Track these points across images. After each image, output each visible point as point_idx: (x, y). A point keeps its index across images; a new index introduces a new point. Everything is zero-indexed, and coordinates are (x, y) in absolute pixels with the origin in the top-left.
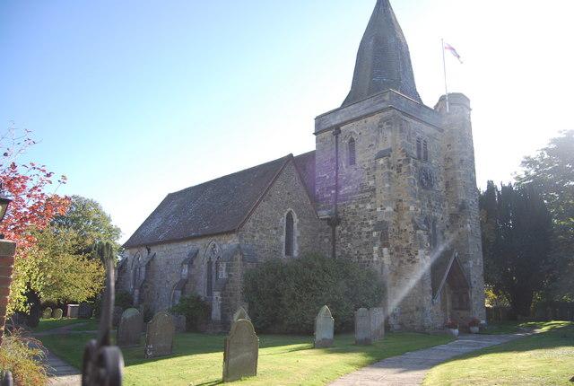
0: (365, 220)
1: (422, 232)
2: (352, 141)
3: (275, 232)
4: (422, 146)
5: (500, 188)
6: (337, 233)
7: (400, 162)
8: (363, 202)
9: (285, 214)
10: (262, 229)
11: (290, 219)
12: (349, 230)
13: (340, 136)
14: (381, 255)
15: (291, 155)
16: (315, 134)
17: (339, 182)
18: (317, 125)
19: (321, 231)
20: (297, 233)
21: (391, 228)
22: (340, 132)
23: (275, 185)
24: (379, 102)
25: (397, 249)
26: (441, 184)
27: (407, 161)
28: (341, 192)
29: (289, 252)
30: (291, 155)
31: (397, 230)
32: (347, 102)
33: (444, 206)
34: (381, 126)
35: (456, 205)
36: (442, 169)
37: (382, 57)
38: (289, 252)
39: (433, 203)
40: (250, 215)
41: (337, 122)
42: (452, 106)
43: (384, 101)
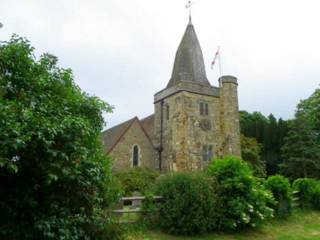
1: (192, 154)
3: (126, 156)
4: (204, 108)
5: (277, 121)
9: (133, 147)
10: (119, 156)
11: (136, 149)
14: (172, 167)
15: (136, 118)
16: (155, 103)
18: (155, 99)
19: (154, 155)
20: (140, 156)
21: (178, 153)
25: (182, 163)
26: (217, 127)
27: (187, 118)
28: (164, 134)
29: (135, 163)
30: (136, 118)
31: (182, 153)
32: (169, 86)
33: (218, 138)
34: (176, 101)
36: (218, 119)
37: (187, 56)
38: (135, 163)
39: (210, 138)
41: (162, 97)
42: (224, 84)
43: (179, 87)
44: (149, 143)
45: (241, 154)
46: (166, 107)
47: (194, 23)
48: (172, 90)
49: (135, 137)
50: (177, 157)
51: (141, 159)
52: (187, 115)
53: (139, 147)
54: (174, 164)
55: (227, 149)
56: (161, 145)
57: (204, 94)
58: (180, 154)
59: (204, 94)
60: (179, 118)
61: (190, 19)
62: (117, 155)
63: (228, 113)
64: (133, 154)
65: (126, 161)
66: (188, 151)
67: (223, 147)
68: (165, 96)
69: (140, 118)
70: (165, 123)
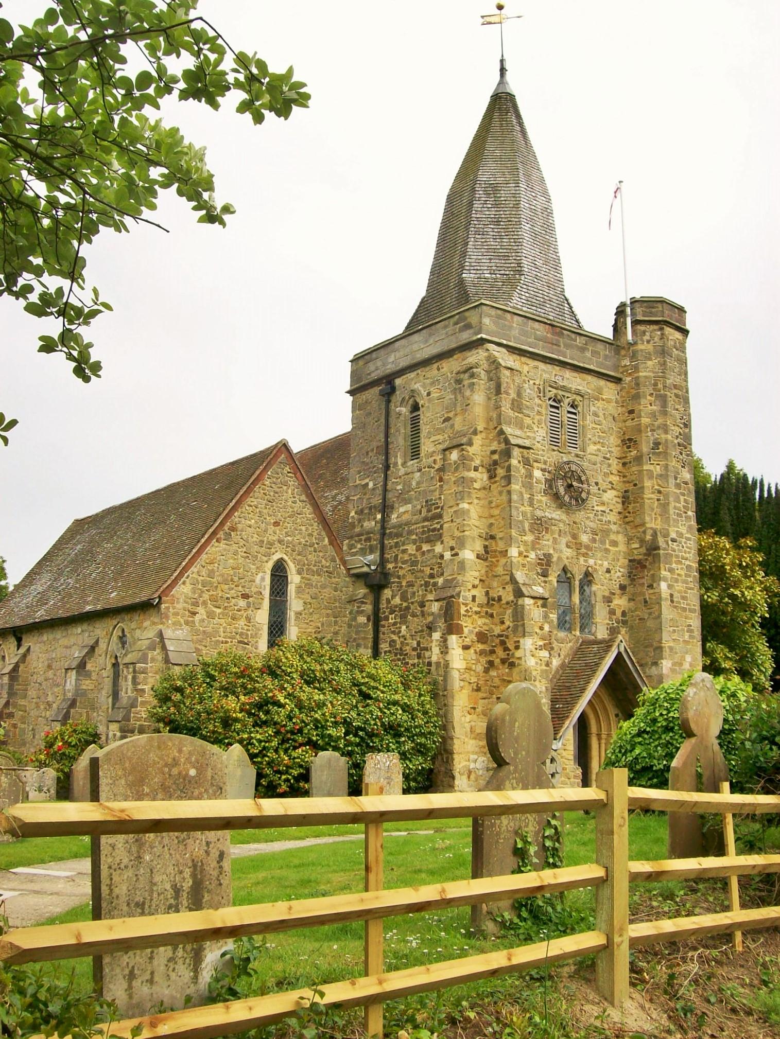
0: (432, 576)
2: (416, 408)
3: (242, 603)
6: (383, 605)
7: (496, 457)
8: (428, 541)
9: (270, 565)
10: (213, 599)
11: (279, 575)
12: (404, 598)
13: (393, 399)
14: (445, 650)
15: (283, 446)
16: (351, 392)
17: (390, 495)
18: (355, 376)
20: (295, 604)
22: (393, 389)
23: (245, 508)
24: (461, 330)
30: (283, 446)
31: (481, 598)
32: (422, 320)
34: (459, 382)
35: (642, 541)
36: (615, 465)
40: (185, 569)
42: (641, 328)
44: (331, 551)
45: (698, 608)
46: (404, 410)
47: (514, 86)
48: (423, 347)
49: (276, 524)
50: (463, 610)
51: (298, 614)
52: (507, 441)
53: (292, 568)
54: (453, 639)
55: (651, 586)
56: (383, 562)
57: (563, 364)
58: (474, 597)
59: (563, 364)
60: (471, 450)
61: (503, 70)
62: (206, 596)
63: (657, 444)
64: (267, 593)
65: (242, 622)
66: (509, 588)
67: (631, 576)
68: (403, 363)
69: (300, 442)
70: (402, 471)
